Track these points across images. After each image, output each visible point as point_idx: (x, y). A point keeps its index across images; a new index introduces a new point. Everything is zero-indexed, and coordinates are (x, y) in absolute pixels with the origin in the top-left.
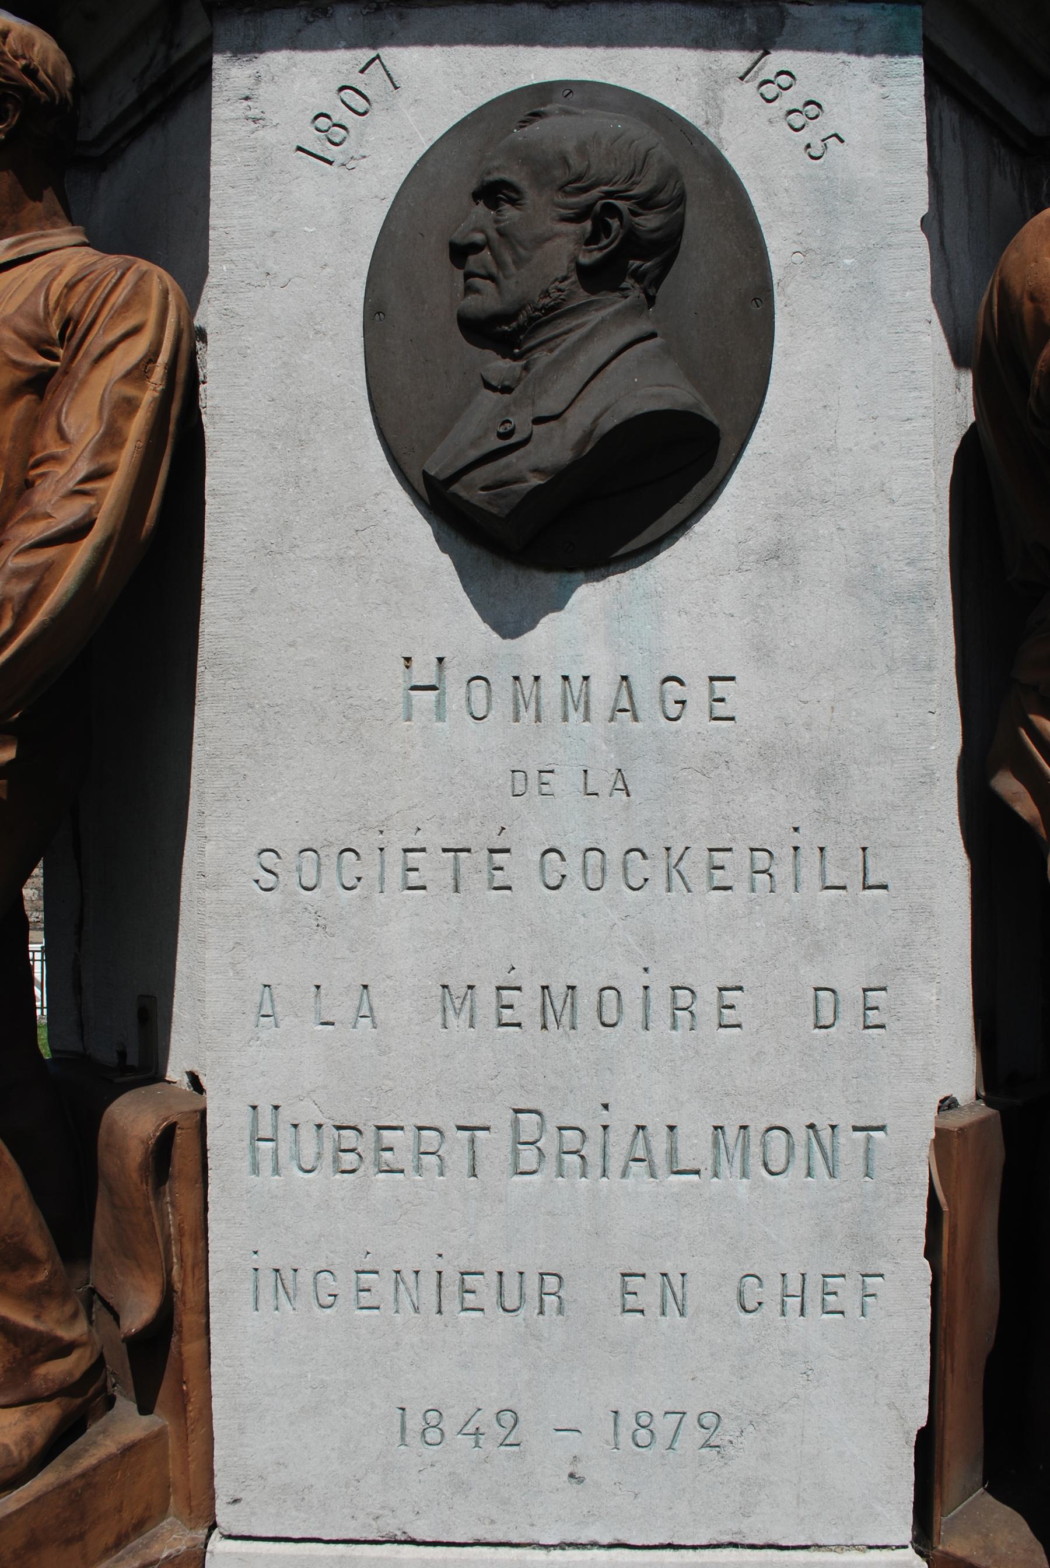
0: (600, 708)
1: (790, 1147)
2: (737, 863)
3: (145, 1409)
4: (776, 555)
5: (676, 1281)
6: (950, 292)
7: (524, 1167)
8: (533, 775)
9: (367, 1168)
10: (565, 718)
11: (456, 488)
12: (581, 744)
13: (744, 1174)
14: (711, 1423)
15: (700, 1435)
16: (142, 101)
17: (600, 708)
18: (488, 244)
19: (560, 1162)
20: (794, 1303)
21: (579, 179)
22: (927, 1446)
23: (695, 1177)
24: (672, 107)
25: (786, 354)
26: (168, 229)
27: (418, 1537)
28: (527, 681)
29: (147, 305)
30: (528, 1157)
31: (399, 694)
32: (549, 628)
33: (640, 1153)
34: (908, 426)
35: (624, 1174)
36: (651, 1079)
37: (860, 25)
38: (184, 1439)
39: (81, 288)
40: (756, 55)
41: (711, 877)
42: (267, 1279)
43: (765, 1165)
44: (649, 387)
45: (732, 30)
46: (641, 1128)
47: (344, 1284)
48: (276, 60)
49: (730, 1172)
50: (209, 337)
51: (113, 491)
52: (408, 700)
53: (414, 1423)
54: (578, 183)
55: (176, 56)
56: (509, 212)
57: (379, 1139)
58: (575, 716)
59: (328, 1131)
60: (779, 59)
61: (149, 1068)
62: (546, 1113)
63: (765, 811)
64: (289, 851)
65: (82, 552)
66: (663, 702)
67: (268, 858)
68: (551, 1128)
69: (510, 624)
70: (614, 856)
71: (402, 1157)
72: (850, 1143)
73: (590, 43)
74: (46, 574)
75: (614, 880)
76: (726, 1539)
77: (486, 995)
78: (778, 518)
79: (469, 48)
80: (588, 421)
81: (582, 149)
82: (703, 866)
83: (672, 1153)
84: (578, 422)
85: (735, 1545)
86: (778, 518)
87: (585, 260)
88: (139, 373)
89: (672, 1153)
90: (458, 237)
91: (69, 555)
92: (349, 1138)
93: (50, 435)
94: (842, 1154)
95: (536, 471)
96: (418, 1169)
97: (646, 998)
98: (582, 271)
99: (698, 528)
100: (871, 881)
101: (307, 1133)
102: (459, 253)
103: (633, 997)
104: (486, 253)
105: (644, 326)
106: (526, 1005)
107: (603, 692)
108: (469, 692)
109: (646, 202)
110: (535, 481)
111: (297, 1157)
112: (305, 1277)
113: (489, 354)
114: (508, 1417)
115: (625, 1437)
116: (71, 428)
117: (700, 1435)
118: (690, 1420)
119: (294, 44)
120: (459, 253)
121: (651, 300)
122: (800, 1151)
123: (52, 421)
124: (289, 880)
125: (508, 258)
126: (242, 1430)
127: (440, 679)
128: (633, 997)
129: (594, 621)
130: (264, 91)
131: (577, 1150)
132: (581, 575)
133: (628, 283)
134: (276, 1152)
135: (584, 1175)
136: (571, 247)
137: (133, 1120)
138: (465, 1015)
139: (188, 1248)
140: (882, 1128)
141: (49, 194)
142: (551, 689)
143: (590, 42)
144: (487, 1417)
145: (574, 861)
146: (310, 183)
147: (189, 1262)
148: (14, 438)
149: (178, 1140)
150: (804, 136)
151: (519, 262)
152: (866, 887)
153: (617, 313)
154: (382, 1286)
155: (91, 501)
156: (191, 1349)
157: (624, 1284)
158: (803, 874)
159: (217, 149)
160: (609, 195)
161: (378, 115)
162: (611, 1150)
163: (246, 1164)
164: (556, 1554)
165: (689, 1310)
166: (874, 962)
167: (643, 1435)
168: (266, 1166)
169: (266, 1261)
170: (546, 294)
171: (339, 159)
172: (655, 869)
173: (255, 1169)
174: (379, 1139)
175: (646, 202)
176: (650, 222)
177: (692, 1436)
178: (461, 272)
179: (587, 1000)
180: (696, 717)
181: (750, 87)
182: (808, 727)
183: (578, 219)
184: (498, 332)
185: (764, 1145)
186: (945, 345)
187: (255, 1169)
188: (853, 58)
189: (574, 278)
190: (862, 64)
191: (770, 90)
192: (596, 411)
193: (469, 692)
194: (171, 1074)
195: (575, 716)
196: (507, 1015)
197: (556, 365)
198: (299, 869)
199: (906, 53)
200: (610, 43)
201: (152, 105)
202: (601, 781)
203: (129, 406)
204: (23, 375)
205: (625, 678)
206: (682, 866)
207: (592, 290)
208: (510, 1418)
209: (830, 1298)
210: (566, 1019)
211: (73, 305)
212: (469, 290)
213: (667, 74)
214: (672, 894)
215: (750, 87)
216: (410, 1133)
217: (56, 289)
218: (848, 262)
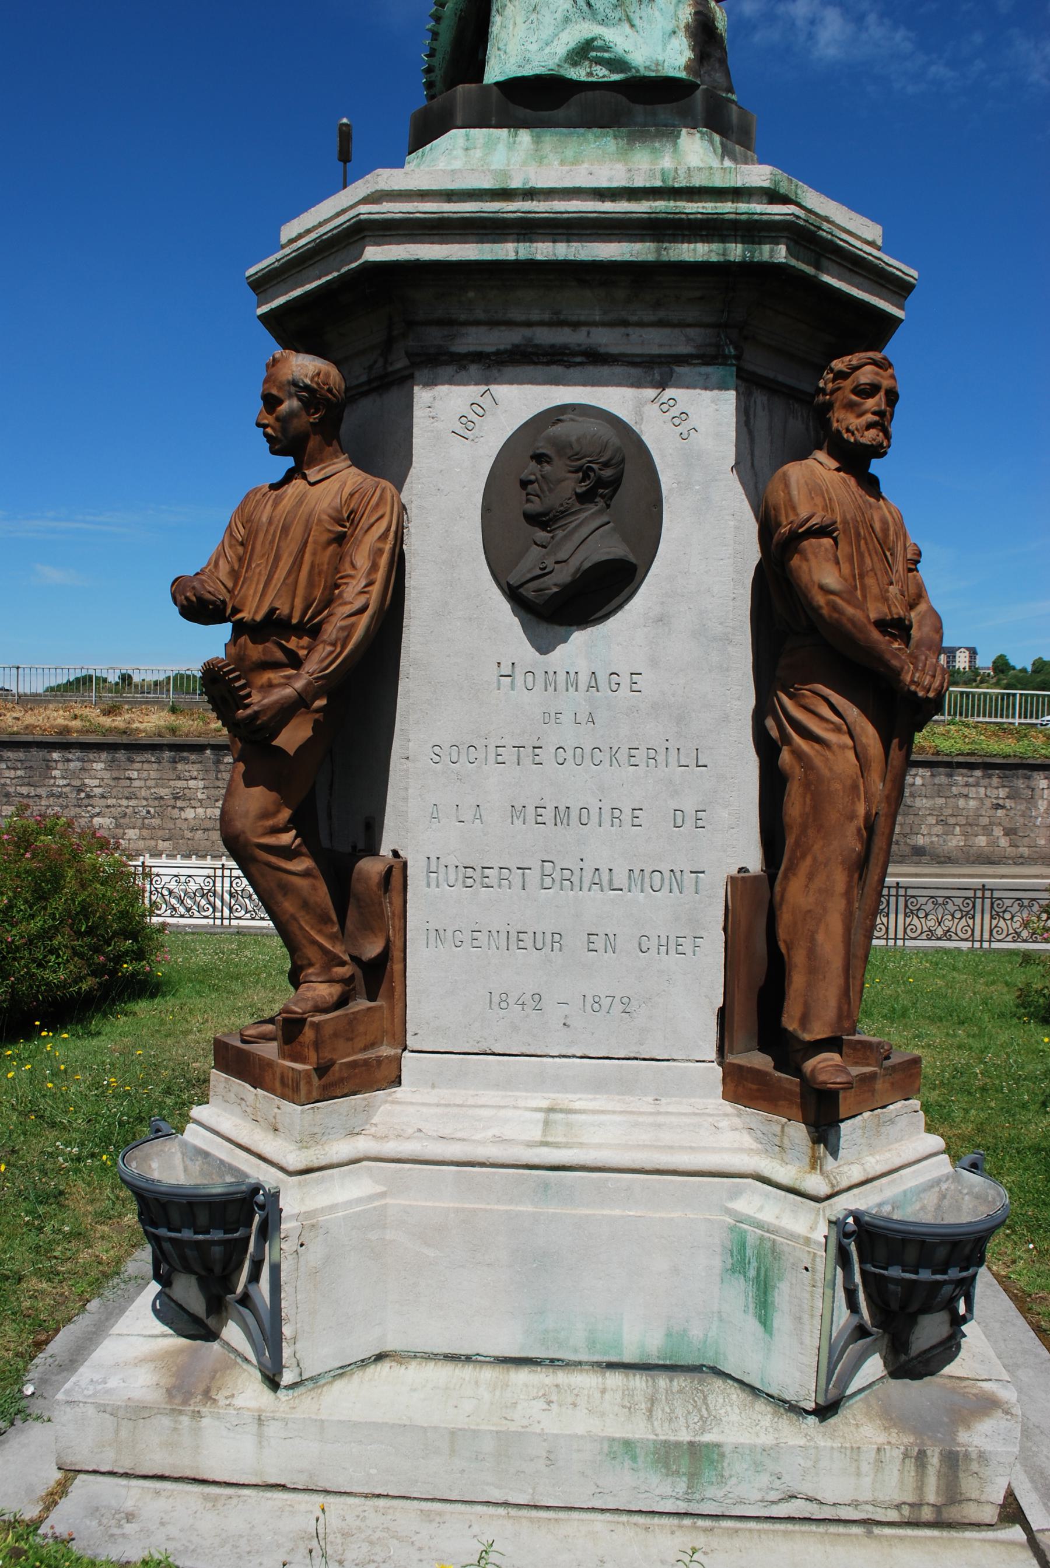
0: (582, 686)
1: (662, 880)
3: (372, 997)
4: (660, 619)
5: (612, 938)
6: (756, 488)
8: (553, 715)
9: (477, 885)
11: (521, 590)
12: (575, 701)
13: (642, 891)
14: (626, 1002)
16: (369, 382)
17: (582, 686)
18: (536, 480)
19: (562, 884)
20: (663, 949)
22: (723, 1015)
24: (620, 416)
25: (668, 529)
26: (387, 455)
27: (496, 1052)
28: (551, 673)
29: (386, 504)
30: (548, 881)
31: (495, 678)
32: (561, 651)
33: (597, 881)
34: (721, 562)
35: (589, 890)
36: (602, 848)
37: (707, 376)
38: (392, 1008)
39: (357, 496)
40: (660, 390)
45: (649, 379)
46: (597, 870)
47: (466, 936)
48: (443, 390)
49: (636, 890)
50: (841, 1152)
51: (376, 589)
52: (499, 681)
53: (496, 999)
54: (576, 456)
55: (390, 369)
56: (547, 468)
57: (483, 873)
58: (571, 689)
59: (461, 868)
60: (670, 392)
61: (372, 849)
64: (446, 746)
65: (364, 619)
67: (437, 750)
68: (558, 869)
69: (544, 648)
70: (587, 751)
72: (689, 879)
73: (584, 385)
75: (587, 760)
76: (632, 1055)
77: (530, 810)
79: (530, 386)
80: (578, 564)
81: (578, 440)
82: (626, 756)
83: (611, 881)
84: (574, 564)
85: (637, 1059)
86: (662, 603)
87: (579, 490)
88: (384, 537)
89: (611, 881)
90: (523, 476)
91: (359, 620)
93: (347, 565)
94: (685, 883)
95: (555, 585)
97: (600, 813)
98: (577, 495)
99: (627, 607)
100: (700, 764)
101: (452, 870)
102: (524, 484)
103: (595, 812)
104: (536, 485)
105: (605, 519)
106: (548, 814)
107: (584, 679)
109: (606, 465)
112: (449, 933)
113: (537, 529)
118: (617, 1000)
119: (451, 382)
120: (524, 484)
121: (608, 506)
122: (667, 882)
123: (348, 559)
125: (546, 488)
126: (419, 1002)
127: (513, 672)
128: (595, 812)
129: (580, 648)
130: (437, 404)
131: (569, 879)
132: (575, 628)
133: (598, 499)
136: (573, 484)
137: (370, 868)
138: (521, 819)
139: (397, 921)
140: (703, 872)
141: (335, 443)
142: (561, 677)
143: (584, 384)
145: (570, 752)
146: (459, 449)
147: (397, 928)
148: (328, 564)
149: (394, 873)
151: (551, 490)
152: (697, 766)
153: (593, 514)
154: (483, 937)
155: (367, 596)
156: (397, 967)
158: (670, 760)
159: (416, 430)
160: (590, 462)
161: (489, 417)
162: (584, 879)
163: (425, 883)
164: (557, 1060)
165: (617, 951)
167: (596, 1007)
168: (433, 884)
169: (432, 926)
170: (562, 505)
171: (471, 437)
172: (605, 757)
173: (428, 885)
174: (483, 873)
175: (606, 465)
176: (607, 473)
177: (618, 1008)
178: (524, 492)
179: (574, 814)
180: (624, 691)
181: (656, 406)
182: (673, 695)
183: (576, 472)
184: (539, 520)
185: (651, 878)
186: (752, 514)
187: (428, 885)
188: (703, 392)
189: (574, 497)
190: (707, 395)
191: (665, 407)
192: (582, 559)
194: (382, 853)
195: (571, 689)
196: (539, 819)
197: (566, 538)
199: (728, 389)
200: (593, 385)
201: (375, 384)
202: (582, 717)
203: (381, 551)
204: (332, 536)
207: (582, 503)
208: (537, 997)
210: (565, 822)
212: (528, 501)
213: (618, 400)
215: (656, 406)
216: (496, 870)
217: (345, 495)
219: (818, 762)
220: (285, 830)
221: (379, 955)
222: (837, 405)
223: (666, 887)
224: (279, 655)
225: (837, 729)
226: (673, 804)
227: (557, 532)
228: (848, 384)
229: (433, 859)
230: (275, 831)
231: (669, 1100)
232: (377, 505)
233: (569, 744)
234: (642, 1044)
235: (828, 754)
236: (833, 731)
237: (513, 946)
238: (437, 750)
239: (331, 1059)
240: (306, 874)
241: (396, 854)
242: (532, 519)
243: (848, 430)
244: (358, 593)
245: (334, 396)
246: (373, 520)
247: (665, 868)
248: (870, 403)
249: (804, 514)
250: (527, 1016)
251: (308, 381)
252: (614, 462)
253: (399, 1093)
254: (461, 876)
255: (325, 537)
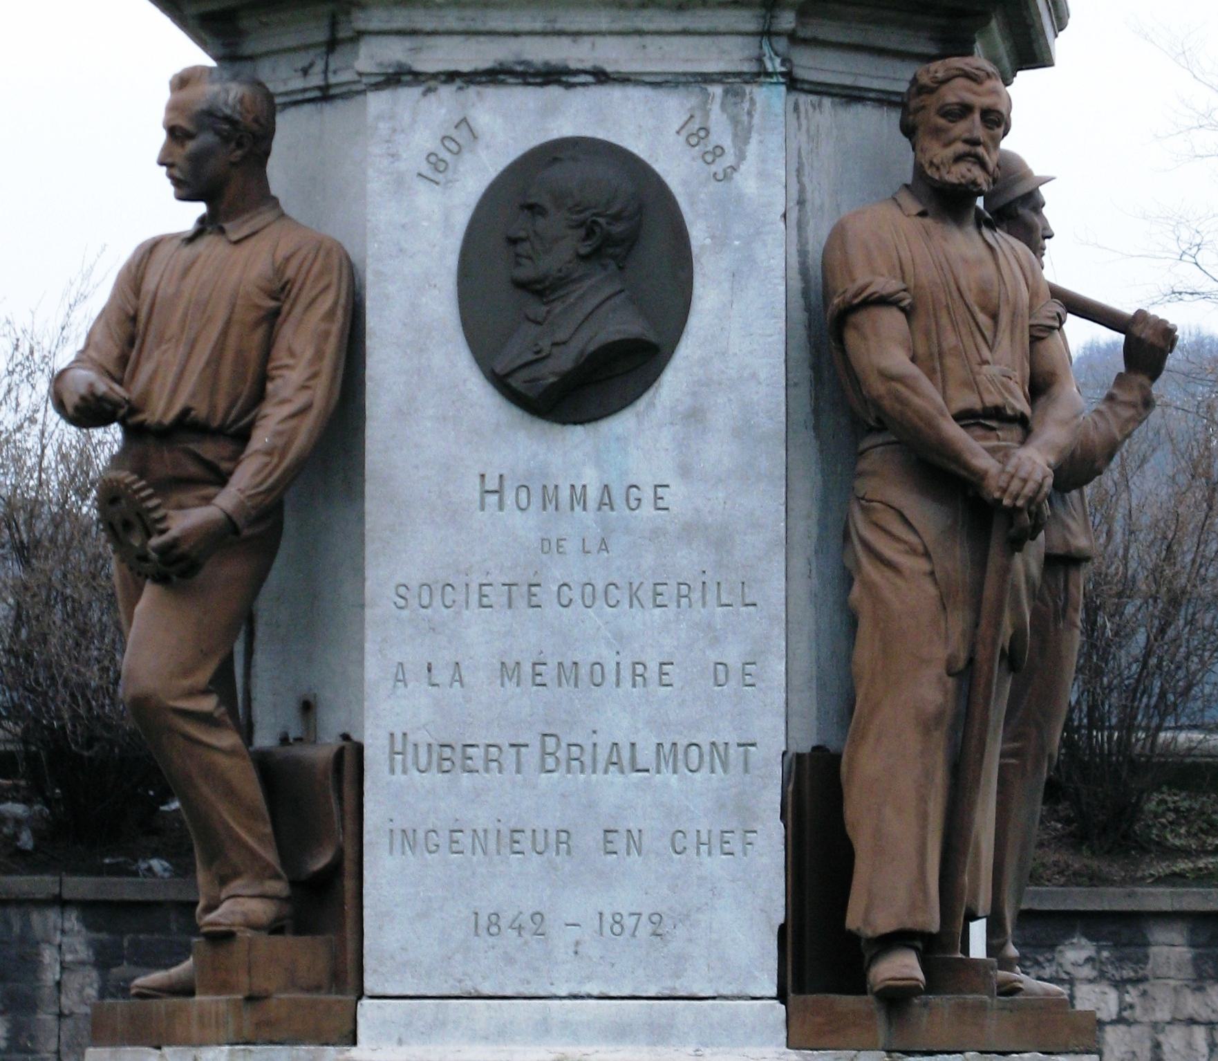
0: (592, 503)
1: (701, 756)
2: (670, 591)
7: (549, 768)
10: (572, 509)
13: (675, 772)
14: (657, 919)
15: (650, 928)
17: (592, 503)
21: (577, 205)
23: (646, 774)
24: (635, 151)
31: (477, 495)
33: (615, 759)
34: (770, 339)
36: (618, 718)
41: (655, 600)
42: (398, 837)
43: (687, 766)
44: (621, 325)
47: (443, 840)
53: (483, 921)
58: (578, 509)
59: (436, 748)
62: (560, 735)
63: (688, 560)
64: (414, 584)
66: (627, 500)
67: (402, 591)
68: (564, 745)
70: (600, 587)
71: (479, 763)
74: (295, 431)
75: (600, 602)
76: (667, 993)
77: (527, 668)
78: (694, 394)
82: (650, 594)
88: (330, 315)
92: (447, 752)
95: (553, 373)
96: (487, 770)
102: (513, 241)
103: (610, 668)
106: (549, 672)
107: (593, 494)
108: (517, 495)
109: (617, 218)
110: (552, 379)
111: (416, 763)
112: (421, 834)
114: (538, 918)
115: (607, 929)
116: (297, 348)
117: (650, 928)
118: (644, 918)
122: (707, 758)
124: (414, 602)
126: (380, 928)
128: (610, 668)
129: (574, 454)
131: (578, 759)
134: (404, 761)
135: (582, 772)
138: (515, 680)
142: (565, 493)
144: (526, 917)
146: (426, 199)
150: (713, 168)
154: (465, 839)
156: (349, 884)
157: (605, 837)
160: (594, 215)
161: (466, 156)
166: (749, 648)
168: (398, 768)
169: (398, 825)
170: (560, 270)
173: (392, 771)
176: (618, 229)
177: (645, 930)
179: (584, 671)
180: (647, 510)
187: (392, 771)
193: (517, 495)
195: (578, 509)
196: (538, 680)
198: (420, 596)
202: (593, 545)
203: (326, 335)
204: (262, 313)
205: (606, 486)
206: (639, 593)
209: (726, 846)
211: (290, 273)
212: (518, 264)
214: (633, 610)
216: (482, 750)
218: (737, 243)
219: (888, 594)
220: (205, 692)
221: (326, 867)
222: (921, 128)
223: (706, 764)
224: (193, 469)
225: (913, 551)
226: (713, 656)
227: (555, 304)
228: (932, 101)
229: (399, 737)
230: (191, 693)
231: (715, 1050)
232: (321, 274)
233: (576, 578)
234: (678, 977)
235: (899, 581)
236: (907, 552)
237: (506, 851)
238: (402, 591)
239: (266, 990)
240: (231, 753)
241: (346, 737)
242: (521, 285)
243: (931, 164)
244: (297, 386)
245: (261, 125)
246: (314, 293)
247: (704, 739)
248: (960, 128)
249: (860, 282)
250: (526, 943)
251: (228, 111)
252: (626, 214)
253: (354, 1052)
254: (435, 757)
255: (252, 316)
